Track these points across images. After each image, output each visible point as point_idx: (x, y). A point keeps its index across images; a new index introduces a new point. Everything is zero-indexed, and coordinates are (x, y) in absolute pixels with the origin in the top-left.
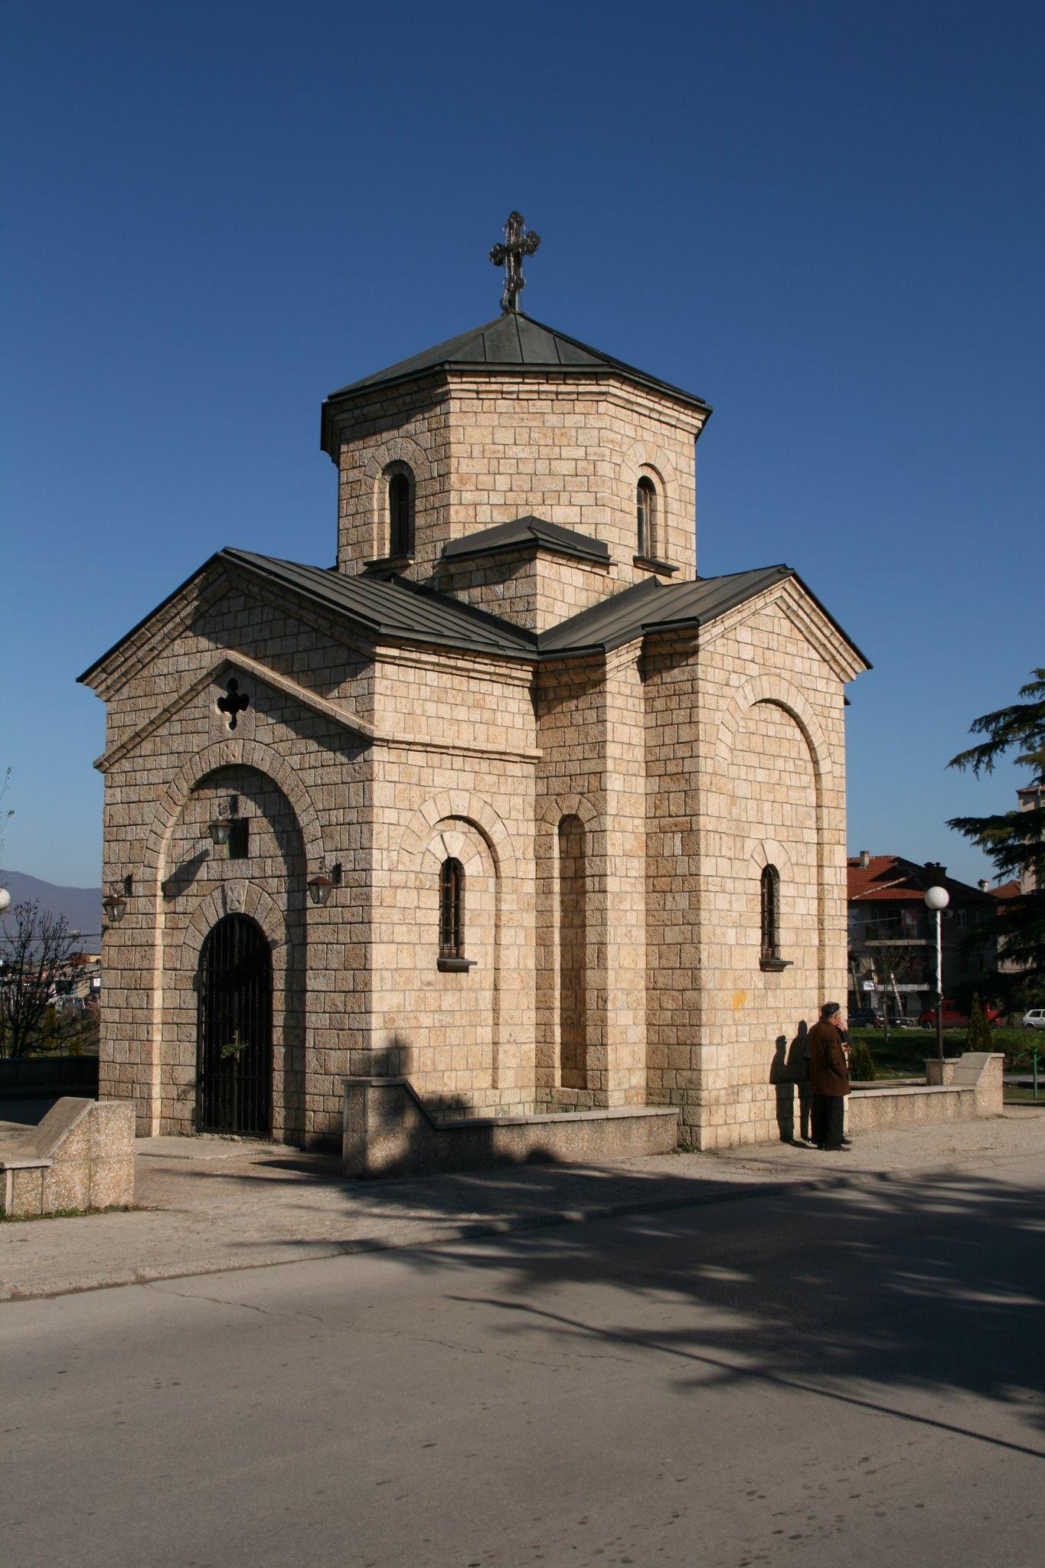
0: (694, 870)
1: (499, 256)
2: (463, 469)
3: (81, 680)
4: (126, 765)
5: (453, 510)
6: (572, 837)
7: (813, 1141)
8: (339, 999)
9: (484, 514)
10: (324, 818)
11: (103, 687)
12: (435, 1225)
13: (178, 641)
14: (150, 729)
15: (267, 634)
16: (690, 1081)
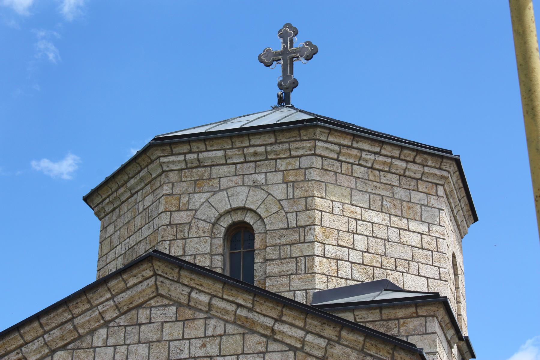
1: (267, 59)
2: (325, 223)
5: (317, 260)
9: (345, 270)
13: (60, 353)
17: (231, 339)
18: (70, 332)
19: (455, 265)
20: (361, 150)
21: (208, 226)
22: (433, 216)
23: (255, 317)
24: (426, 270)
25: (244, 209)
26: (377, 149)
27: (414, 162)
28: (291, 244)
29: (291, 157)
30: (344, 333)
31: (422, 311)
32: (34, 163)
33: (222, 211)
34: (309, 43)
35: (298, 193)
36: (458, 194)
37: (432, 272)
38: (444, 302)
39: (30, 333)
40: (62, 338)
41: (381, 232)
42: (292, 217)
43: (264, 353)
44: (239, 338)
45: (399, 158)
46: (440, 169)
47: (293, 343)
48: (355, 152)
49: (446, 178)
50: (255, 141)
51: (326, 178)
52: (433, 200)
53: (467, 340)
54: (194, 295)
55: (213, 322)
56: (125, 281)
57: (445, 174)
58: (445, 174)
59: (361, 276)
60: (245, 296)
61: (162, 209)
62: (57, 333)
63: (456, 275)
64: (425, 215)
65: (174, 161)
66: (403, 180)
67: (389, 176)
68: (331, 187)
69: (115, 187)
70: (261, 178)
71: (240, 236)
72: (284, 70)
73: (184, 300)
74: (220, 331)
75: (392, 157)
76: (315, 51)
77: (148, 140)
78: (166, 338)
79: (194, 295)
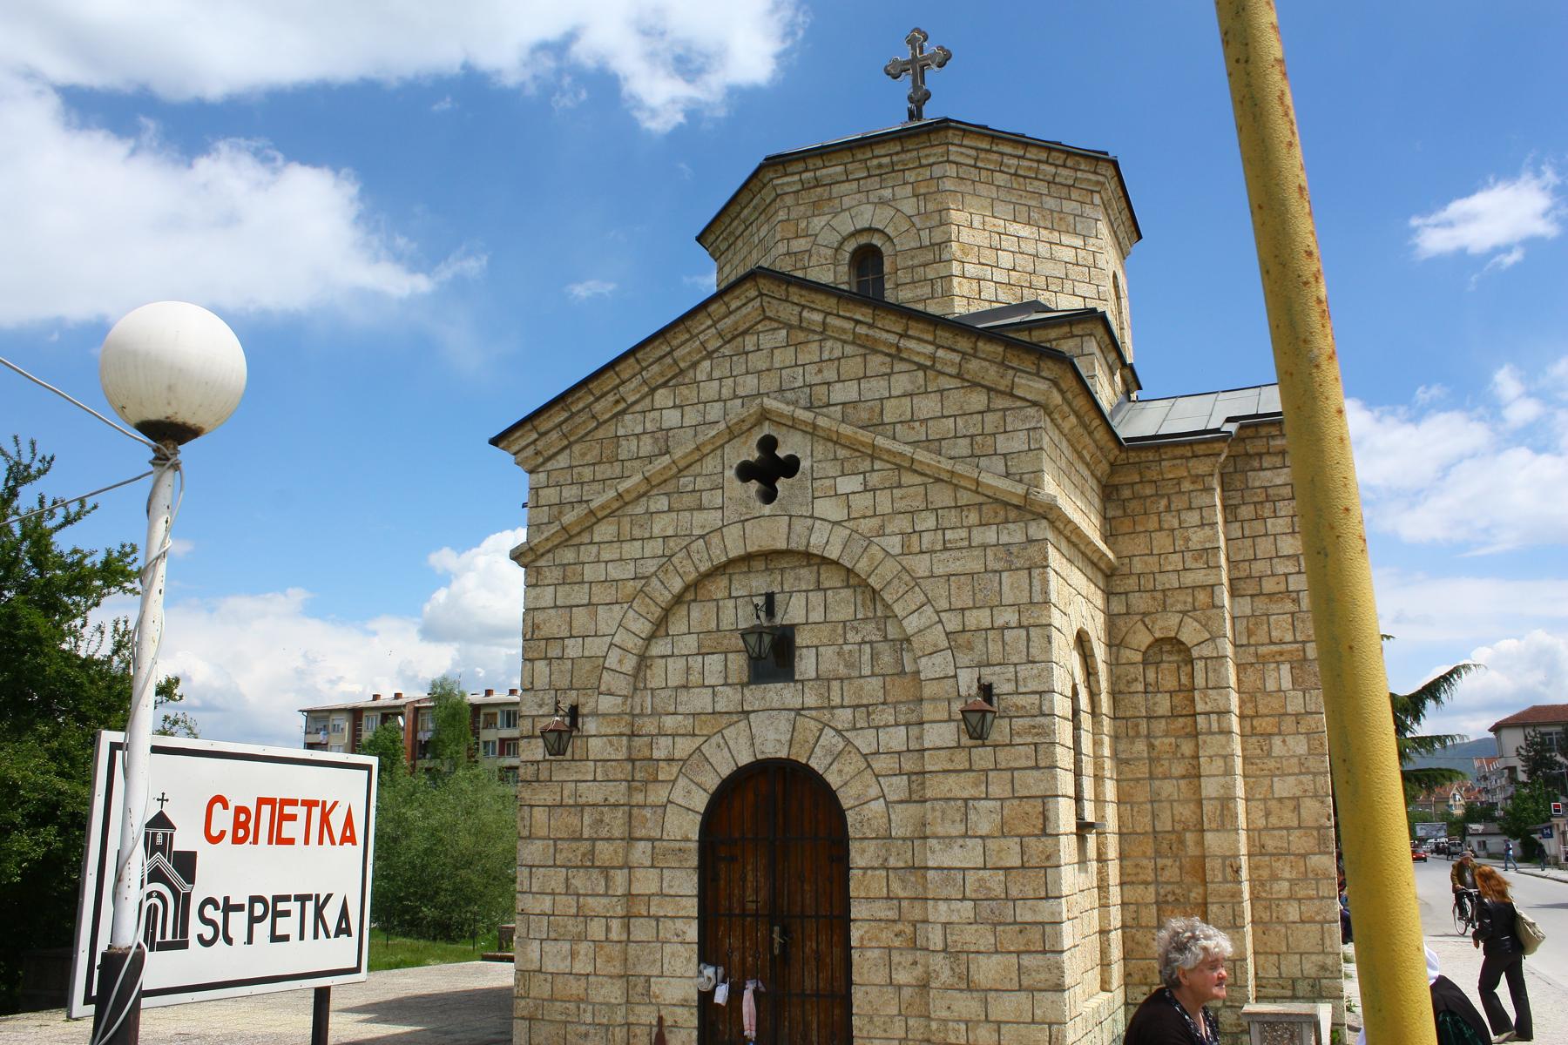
3: (495, 442)
4: (568, 555)
5: (955, 281)
6: (1165, 665)
8: (995, 881)
9: (988, 291)
10: (953, 623)
11: (530, 451)
13: (660, 391)
14: (615, 505)
15: (830, 374)
16: (1323, 968)
17: (851, 362)
18: (670, 366)
19: (1116, 287)
20: (1002, 154)
21: (830, 252)
22: (1089, 228)
24: (1083, 289)
25: (871, 230)
26: (1021, 153)
27: (1064, 166)
28: (925, 265)
29: (921, 166)
30: (980, 344)
31: (1077, 330)
32: (685, 280)
33: (845, 234)
34: (942, 48)
35: (931, 207)
36: (1117, 205)
37: (1088, 290)
38: (1103, 318)
39: (626, 370)
40: (662, 374)
41: (1029, 247)
42: (925, 234)
43: (889, 375)
44: (859, 359)
45: (1047, 162)
46: (1095, 173)
47: (921, 360)
48: (995, 157)
49: (1103, 184)
50: (879, 151)
51: (962, 188)
52: (1088, 210)
53: (1131, 367)
54: (805, 314)
55: (829, 344)
56: (727, 305)
57: (1101, 179)
58: (1101, 179)
59: (1006, 297)
60: (864, 310)
61: (778, 237)
62: (655, 368)
63: (1118, 298)
64: (1079, 227)
65: (789, 182)
66: (1053, 188)
67: (1036, 183)
69: (727, 221)
70: (887, 193)
71: (867, 259)
72: (915, 81)
73: (795, 321)
74: (837, 353)
75: (1039, 161)
76: (948, 56)
77: (761, 160)
78: (777, 365)
79: (805, 314)
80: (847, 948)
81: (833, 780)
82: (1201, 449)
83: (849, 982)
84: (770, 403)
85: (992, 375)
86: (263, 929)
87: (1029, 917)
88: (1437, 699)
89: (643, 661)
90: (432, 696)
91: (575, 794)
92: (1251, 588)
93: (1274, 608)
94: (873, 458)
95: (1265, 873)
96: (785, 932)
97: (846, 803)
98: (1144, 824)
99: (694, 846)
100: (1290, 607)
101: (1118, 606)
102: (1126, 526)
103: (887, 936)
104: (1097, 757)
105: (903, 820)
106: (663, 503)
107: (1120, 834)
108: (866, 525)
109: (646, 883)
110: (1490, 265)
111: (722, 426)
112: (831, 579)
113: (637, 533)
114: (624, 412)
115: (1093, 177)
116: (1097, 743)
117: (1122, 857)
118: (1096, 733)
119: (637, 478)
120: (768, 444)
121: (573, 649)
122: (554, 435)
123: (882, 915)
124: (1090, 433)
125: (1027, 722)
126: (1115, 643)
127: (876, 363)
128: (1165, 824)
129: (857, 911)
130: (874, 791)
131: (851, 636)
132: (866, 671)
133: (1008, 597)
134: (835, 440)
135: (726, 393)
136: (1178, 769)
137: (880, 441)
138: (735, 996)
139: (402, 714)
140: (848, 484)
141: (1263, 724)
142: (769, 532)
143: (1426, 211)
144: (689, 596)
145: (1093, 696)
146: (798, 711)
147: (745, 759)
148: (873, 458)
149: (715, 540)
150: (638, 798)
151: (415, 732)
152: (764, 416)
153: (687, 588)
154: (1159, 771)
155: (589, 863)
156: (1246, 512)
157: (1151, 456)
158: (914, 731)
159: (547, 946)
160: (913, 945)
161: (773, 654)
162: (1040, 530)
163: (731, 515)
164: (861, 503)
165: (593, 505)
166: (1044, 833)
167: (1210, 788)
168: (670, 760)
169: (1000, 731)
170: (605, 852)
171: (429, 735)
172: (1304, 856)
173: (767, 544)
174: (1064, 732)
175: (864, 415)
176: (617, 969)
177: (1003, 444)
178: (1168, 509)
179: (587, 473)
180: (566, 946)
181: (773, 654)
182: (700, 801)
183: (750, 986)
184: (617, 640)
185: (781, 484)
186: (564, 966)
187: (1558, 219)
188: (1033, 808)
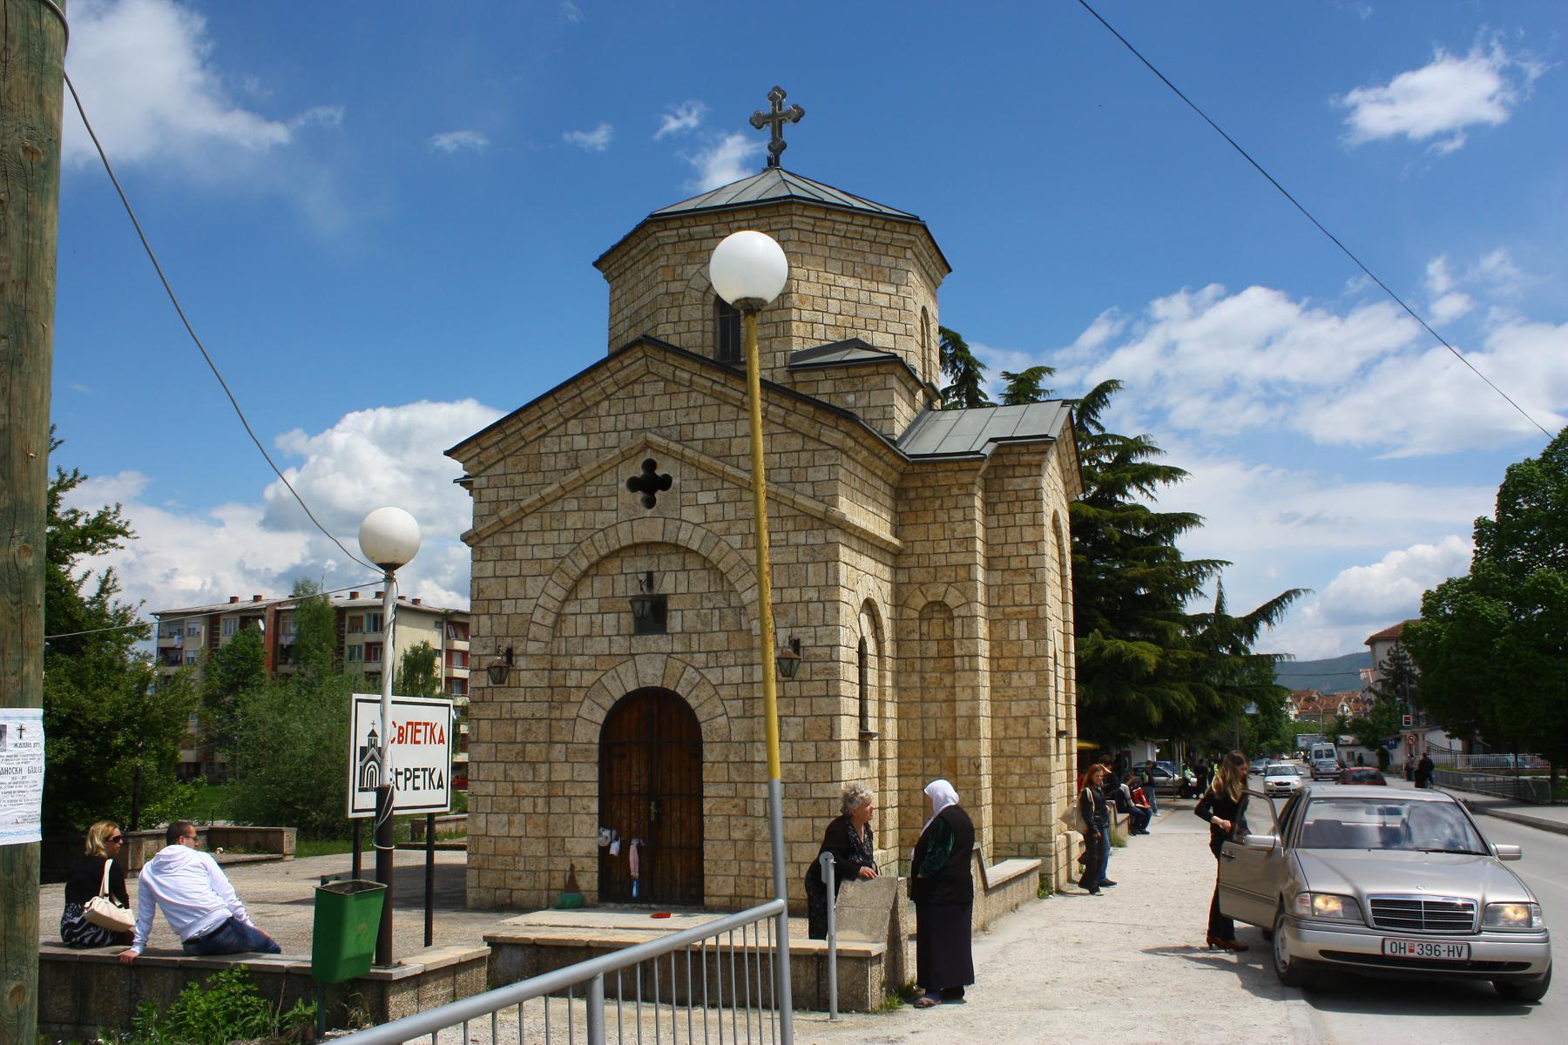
0: (1040, 653)
3: (448, 453)
4: (505, 540)
5: (794, 325)
7: (1082, 884)
9: (819, 332)
12: (1444, 945)
15: (695, 418)
16: (1039, 836)
17: (710, 409)
21: (700, 295)
23: (729, 391)
24: (894, 327)
31: (882, 370)
32: (566, 136)
34: (796, 107)
39: (547, 405)
41: (852, 296)
48: (829, 224)
51: (802, 250)
52: (901, 263)
59: (834, 337)
62: (568, 405)
65: (668, 235)
68: (806, 258)
72: (773, 133)
74: (700, 402)
76: (801, 114)
80: (701, 816)
81: (692, 702)
82: (965, 466)
83: (702, 839)
84: (651, 437)
85: (806, 426)
86: (410, 783)
87: (820, 794)
88: (1269, 621)
89: (560, 617)
90: (294, 599)
91: (511, 711)
92: (1002, 564)
93: (1018, 580)
94: (723, 480)
95: (1003, 770)
96: (658, 806)
97: (701, 718)
98: (916, 733)
99: (596, 747)
100: (1028, 579)
101: (903, 577)
102: (911, 519)
103: (727, 808)
104: (881, 687)
105: (739, 730)
106: (574, 505)
107: (899, 741)
108: (717, 527)
109: (562, 773)
110: (1428, 150)
111: (617, 451)
112: (692, 563)
113: (555, 525)
114: (545, 435)
115: (905, 237)
116: (881, 677)
117: (900, 757)
118: (881, 669)
119: (555, 486)
120: (650, 465)
121: (508, 607)
122: (493, 451)
123: (724, 793)
124: (880, 458)
125: (821, 665)
126: (899, 603)
127: (727, 410)
128: (931, 733)
129: (708, 791)
130: (720, 710)
131: (706, 604)
132: (716, 628)
133: (812, 581)
134: (697, 466)
135: (620, 426)
136: (941, 695)
137: (728, 469)
138: (624, 849)
139: (262, 617)
140: (705, 498)
141: (1007, 664)
142: (651, 529)
143: (1365, 83)
144: (593, 572)
145: (879, 644)
146: (669, 655)
147: (632, 687)
148: (723, 480)
149: (612, 533)
150: (556, 714)
151: (276, 636)
152: (647, 445)
153: (591, 566)
154: (928, 696)
155: (521, 759)
156: (1001, 508)
157: (929, 469)
158: (747, 670)
159: (492, 818)
160: (745, 813)
161: (651, 614)
162: (831, 536)
163: (622, 515)
164: (715, 511)
165: (524, 504)
166: (831, 739)
167: (962, 709)
168: (579, 687)
169: (804, 671)
170: (533, 751)
171: (291, 639)
172: (1030, 758)
173: (649, 538)
174: (852, 673)
175: (718, 449)
176: (542, 833)
177: (812, 475)
178: (941, 508)
179: (518, 479)
180: (505, 818)
181: (651, 614)
182: (600, 716)
183: (634, 843)
184: (541, 602)
185: (659, 495)
186: (504, 831)
187: (1503, 103)
188: (824, 722)
